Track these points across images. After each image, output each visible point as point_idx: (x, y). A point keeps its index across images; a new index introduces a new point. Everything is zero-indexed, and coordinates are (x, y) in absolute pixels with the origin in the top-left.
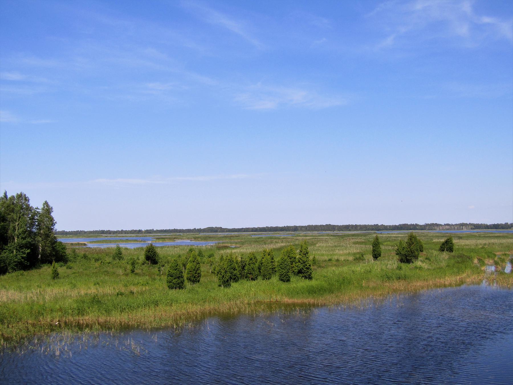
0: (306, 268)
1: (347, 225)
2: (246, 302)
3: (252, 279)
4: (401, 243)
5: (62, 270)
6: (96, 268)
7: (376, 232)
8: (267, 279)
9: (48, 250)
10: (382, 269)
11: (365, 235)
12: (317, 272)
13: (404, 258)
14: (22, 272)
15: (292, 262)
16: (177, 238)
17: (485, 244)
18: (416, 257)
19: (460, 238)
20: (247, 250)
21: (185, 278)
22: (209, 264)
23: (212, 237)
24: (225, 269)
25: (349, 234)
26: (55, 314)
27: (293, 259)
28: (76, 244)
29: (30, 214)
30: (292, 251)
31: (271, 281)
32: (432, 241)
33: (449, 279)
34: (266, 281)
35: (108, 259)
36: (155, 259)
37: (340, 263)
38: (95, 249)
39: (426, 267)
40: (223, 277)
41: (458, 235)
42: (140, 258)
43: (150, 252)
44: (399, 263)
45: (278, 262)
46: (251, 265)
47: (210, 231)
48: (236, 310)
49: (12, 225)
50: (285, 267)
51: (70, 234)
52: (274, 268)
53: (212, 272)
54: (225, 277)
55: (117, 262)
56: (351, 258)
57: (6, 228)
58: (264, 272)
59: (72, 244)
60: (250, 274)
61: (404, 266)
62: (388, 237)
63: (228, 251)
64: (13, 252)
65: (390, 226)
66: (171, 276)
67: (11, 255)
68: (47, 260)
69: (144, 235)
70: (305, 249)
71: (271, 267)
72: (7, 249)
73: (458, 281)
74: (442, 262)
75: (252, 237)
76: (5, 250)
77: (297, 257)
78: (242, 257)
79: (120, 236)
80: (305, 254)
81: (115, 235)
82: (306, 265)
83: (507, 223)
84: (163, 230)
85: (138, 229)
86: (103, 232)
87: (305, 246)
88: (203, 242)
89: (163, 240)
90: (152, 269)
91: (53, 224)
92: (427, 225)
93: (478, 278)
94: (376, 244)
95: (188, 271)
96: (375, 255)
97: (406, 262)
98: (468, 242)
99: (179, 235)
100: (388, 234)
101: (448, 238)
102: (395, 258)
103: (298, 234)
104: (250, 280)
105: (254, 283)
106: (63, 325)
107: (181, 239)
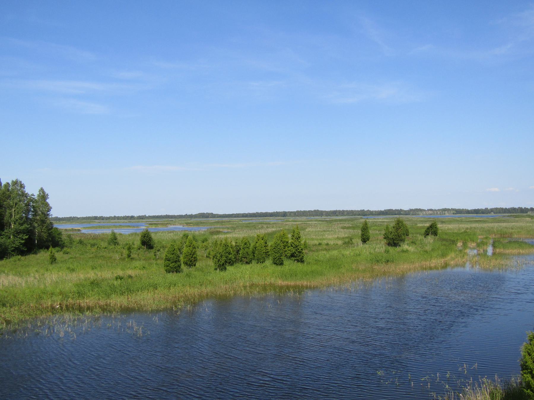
0: (298, 252)
1: (335, 211)
2: (242, 284)
3: (247, 263)
4: (387, 227)
5: (59, 255)
6: (92, 253)
7: (362, 217)
8: (260, 263)
9: (45, 236)
10: (370, 253)
11: (352, 220)
12: (309, 256)
13: (391, 242)
14: (19, 257)
15: (284, 246)
16: (169, 224)
17: (467, 229)
18: (403, 240)
19: (443, 222)
20: (240, 235)
21: (182, 263)
22: (204, 249)
23: (204, 223)
24: (221, 254)
25: (337, 219)
26: (54, 298)
27: (285, 243)
28: (70, 230)
29: (26, 201)
30: (285, 236)
31: (264, 264)
32: (417, 226)
33: (436, 262)
34: (260, 264)
35: (104, 244)
36: (150, 244)
37: (330, 247)
38: (90, 235)
39: (412, 250)
40: (219, 261)
41: (441, 220)
42: (135, 243)
43: (146, 238)
44: (387, 246)
45: (271, 246)
46: (246, 249)
47: (201, 217)
48: (232, 293)
49: (8, 211)
50: (278, 251)
51: (63, 220)
52: (268, 252)
53: (207, 257)
54: (220, 261)
55: (113, 247)
56: (340, 242)
57: (2, 214)
58: (258, 256)
59: (66, 230)
60: (245, 258)
61: (391, 249)
62: (374, 222)
63: (222, 236)
64: (10, 238)
65: (375, 211)
66: (168, 260)
67: (9, 240)
68: (44, 245)
69: (137, 220)
70: (297, 234)
71: (264, 251)
72: (4, 235)
73: (443, 264)
74: (426, 246)
75: (243, 222)
76: (2, 235)
77: (290, 241)
78: (236, 241)
79: (113, 222)
80: (298, 239)
81: (108, 221)
82: (298, 249)
83: (488, 208)
84: (156, 216)
85: (130, 215)
86: (96, 218)
87: (297, 231)
88: (195, 227)
89: (156, 225)
90: (148, 253)
91: (49, 209)
92: (411, 210)
93: (462, 260)
94: (365, 229)
95: (185, 255)
96: (364, 239)
97: (393, 246)
98: (451, 226)
99: (172, 221)
100: (375, 219)
101: (433, 223)
102: (383, 242)
103: (288, 220)
104: (244, 264)
105: (248, 266)
106: (64, 307)
107: (174, 225)
